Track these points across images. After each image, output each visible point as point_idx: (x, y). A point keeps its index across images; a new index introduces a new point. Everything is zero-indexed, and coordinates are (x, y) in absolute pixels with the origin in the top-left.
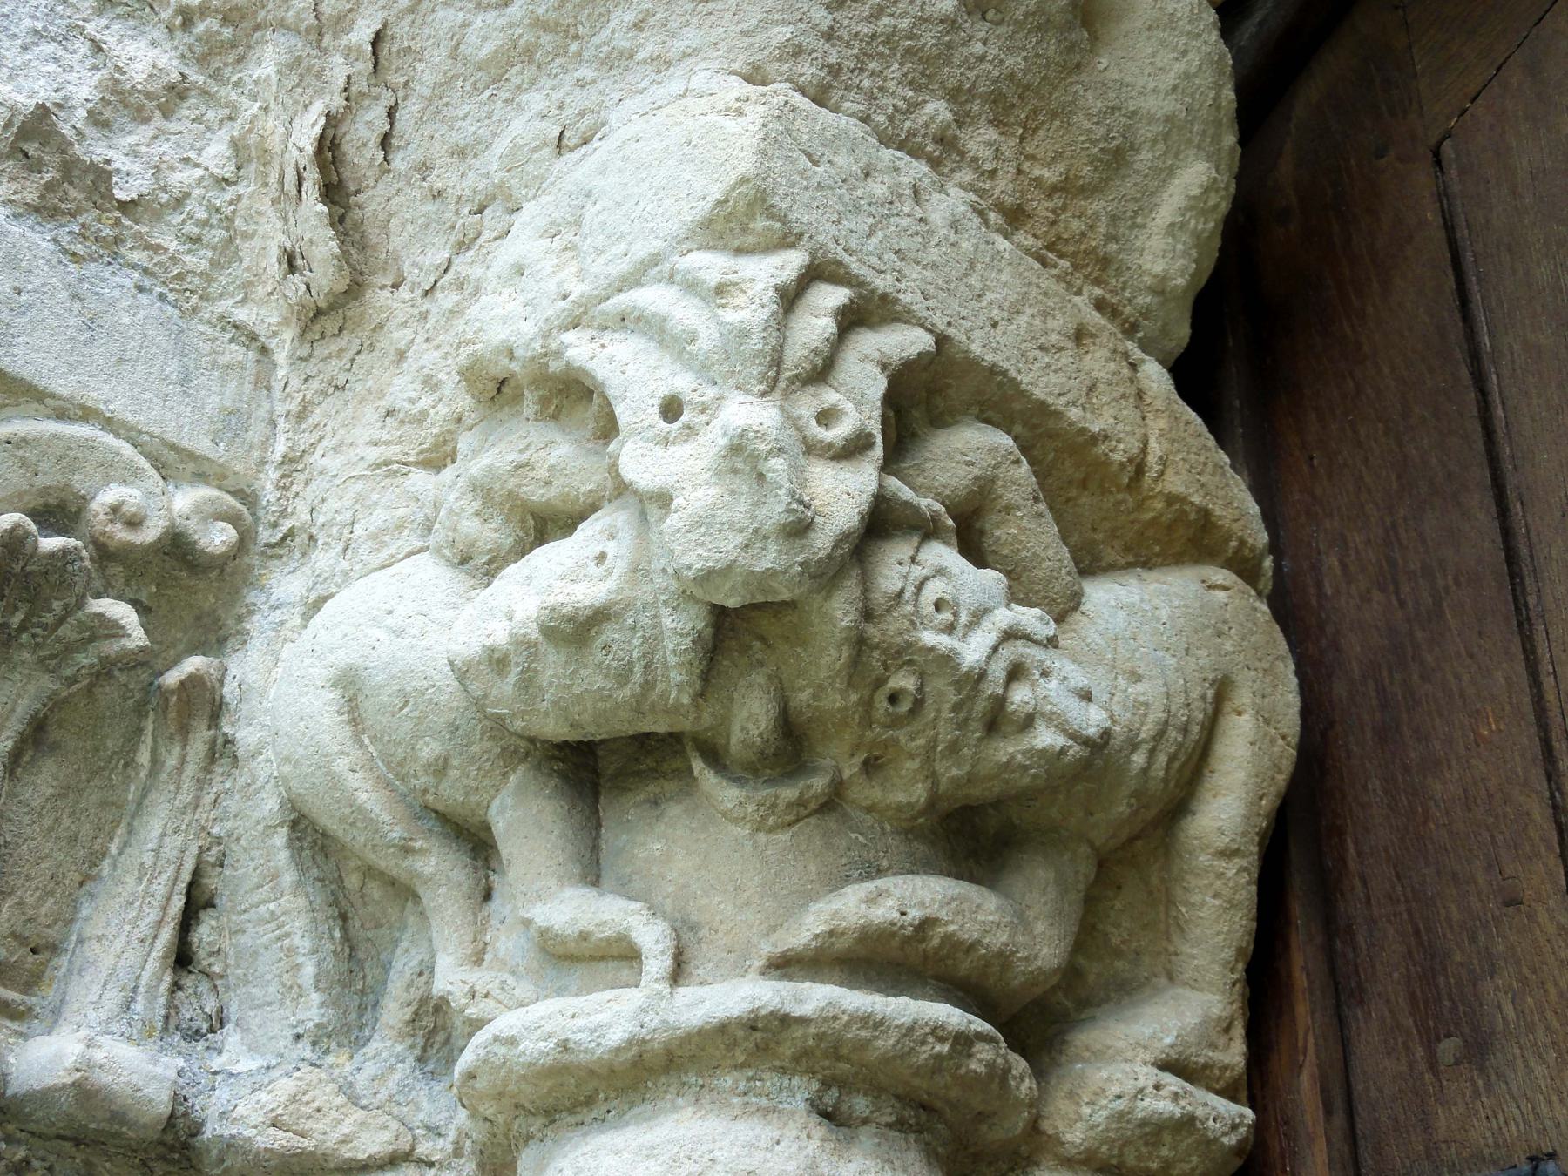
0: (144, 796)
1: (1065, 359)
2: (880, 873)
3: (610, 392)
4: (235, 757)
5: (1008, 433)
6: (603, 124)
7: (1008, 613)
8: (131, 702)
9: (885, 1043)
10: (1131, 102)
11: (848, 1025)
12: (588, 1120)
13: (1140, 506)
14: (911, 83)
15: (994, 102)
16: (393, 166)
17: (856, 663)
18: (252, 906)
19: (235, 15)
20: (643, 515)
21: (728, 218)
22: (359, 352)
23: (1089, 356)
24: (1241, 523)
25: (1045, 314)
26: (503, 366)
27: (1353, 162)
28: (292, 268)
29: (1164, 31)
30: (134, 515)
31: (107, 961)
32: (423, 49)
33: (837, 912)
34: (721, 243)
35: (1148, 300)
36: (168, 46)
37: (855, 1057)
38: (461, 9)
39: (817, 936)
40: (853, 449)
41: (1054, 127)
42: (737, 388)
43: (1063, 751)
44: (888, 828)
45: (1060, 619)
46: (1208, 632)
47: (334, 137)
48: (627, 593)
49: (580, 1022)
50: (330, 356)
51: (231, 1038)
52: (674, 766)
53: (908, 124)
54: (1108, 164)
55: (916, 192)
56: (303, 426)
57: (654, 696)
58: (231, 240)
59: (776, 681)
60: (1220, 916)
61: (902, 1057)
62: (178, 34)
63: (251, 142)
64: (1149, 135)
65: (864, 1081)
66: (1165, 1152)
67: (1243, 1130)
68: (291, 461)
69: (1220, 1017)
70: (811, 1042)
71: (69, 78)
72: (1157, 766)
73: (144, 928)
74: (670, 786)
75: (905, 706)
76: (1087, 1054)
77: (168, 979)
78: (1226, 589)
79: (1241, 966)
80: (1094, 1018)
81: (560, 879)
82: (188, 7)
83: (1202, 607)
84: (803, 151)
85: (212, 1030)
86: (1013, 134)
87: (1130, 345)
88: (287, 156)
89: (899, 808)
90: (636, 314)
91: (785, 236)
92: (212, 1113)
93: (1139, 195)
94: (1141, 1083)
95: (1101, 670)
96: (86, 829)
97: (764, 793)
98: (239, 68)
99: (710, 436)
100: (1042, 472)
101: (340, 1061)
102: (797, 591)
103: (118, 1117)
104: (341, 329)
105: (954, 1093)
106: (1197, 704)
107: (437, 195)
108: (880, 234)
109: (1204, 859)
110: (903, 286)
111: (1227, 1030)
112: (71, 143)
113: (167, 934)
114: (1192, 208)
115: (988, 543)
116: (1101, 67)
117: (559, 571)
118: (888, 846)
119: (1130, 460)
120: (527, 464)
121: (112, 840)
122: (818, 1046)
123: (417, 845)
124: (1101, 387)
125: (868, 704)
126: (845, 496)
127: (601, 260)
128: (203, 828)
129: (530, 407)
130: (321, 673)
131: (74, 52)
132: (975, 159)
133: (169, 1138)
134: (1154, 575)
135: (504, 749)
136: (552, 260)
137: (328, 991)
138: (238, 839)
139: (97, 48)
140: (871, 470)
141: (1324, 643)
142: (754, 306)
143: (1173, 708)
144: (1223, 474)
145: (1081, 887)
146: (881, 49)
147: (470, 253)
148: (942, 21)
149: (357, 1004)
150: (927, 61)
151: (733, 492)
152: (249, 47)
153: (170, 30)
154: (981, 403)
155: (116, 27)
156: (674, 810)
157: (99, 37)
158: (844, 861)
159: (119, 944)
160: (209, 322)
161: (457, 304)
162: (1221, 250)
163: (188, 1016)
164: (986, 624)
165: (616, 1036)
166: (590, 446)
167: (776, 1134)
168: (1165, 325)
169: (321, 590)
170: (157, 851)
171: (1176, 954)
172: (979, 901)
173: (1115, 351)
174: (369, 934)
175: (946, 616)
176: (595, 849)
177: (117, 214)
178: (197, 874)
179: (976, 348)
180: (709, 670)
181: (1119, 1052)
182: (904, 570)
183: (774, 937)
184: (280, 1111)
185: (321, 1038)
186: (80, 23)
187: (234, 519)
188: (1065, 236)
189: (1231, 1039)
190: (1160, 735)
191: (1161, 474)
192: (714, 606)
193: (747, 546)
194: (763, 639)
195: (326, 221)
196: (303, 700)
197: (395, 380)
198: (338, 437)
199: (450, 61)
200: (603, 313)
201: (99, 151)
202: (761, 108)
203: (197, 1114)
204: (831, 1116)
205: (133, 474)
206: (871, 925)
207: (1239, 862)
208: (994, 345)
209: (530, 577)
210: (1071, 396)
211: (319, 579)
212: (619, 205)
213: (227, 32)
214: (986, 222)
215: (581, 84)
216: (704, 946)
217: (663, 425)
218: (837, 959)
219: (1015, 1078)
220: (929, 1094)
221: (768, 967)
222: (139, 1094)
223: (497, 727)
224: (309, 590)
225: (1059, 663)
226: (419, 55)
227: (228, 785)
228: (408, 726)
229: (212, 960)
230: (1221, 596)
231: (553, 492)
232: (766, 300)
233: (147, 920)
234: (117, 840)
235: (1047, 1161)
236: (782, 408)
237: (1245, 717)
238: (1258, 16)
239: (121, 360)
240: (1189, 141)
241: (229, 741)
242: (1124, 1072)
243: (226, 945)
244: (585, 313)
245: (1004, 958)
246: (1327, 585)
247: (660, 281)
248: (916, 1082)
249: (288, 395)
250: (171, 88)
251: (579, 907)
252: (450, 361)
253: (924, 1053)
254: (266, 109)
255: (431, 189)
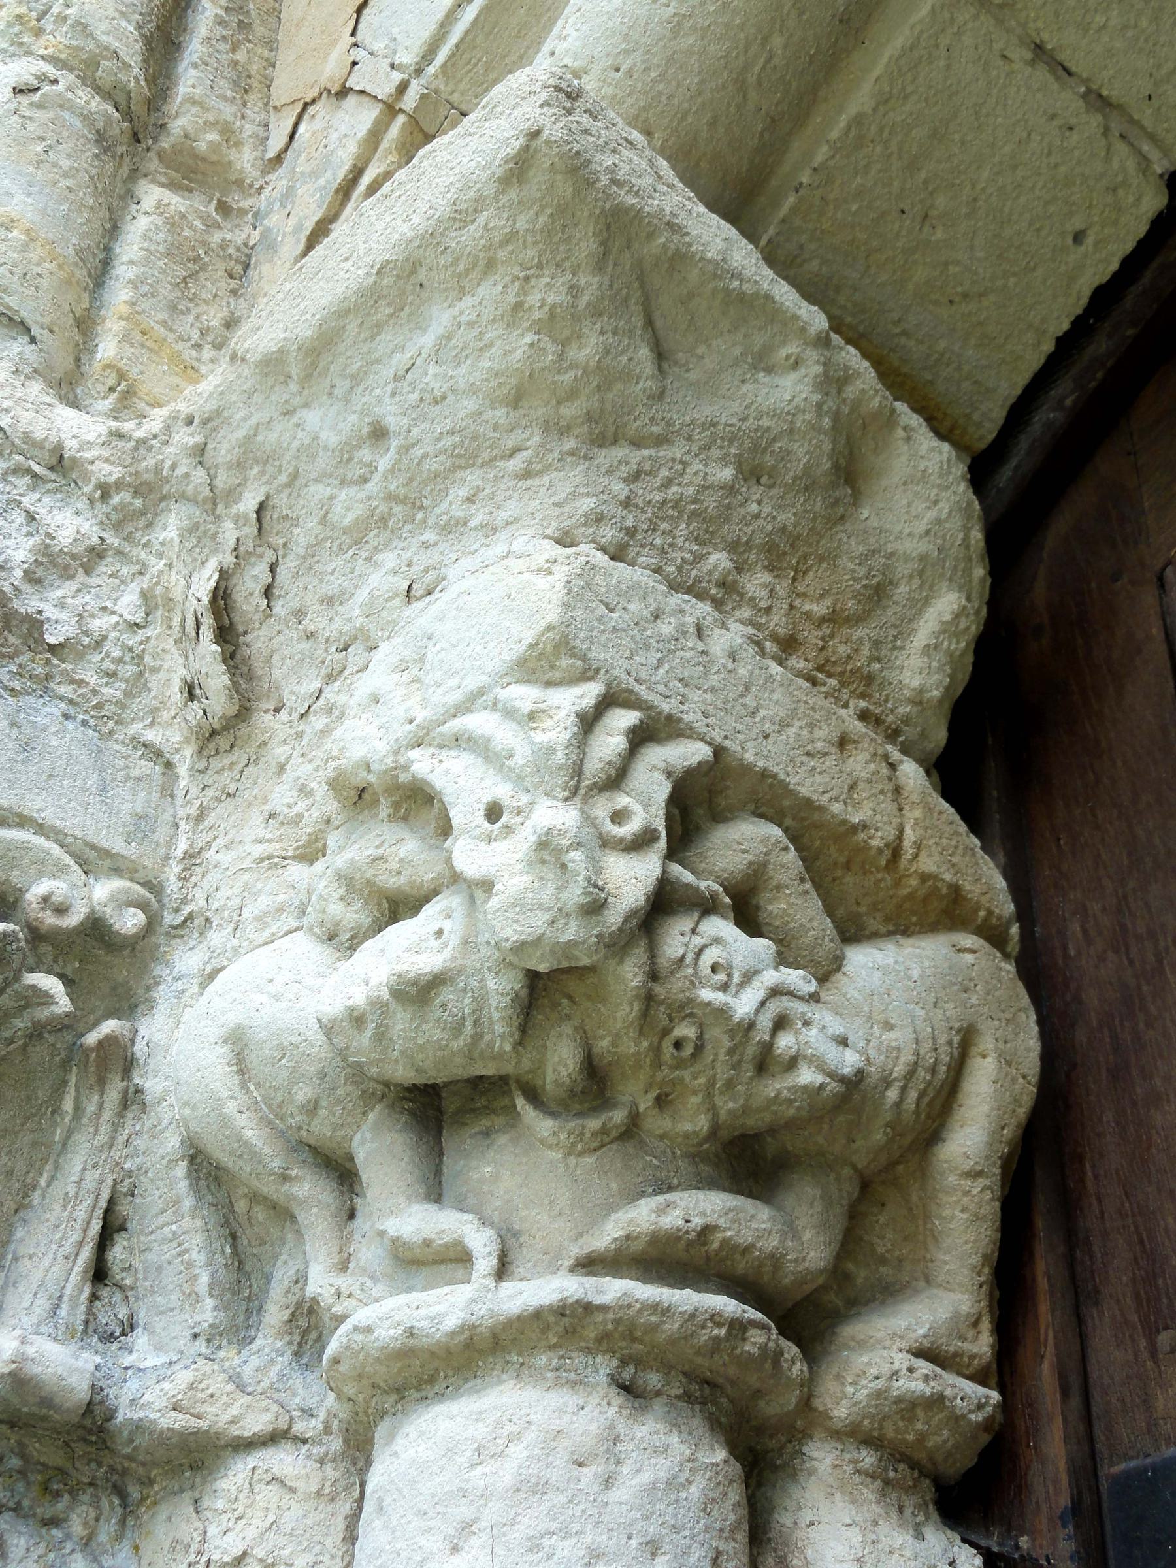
0: (68, 1137)
1: (829, 762)
2: (671, 1189)
3: (446, 799)
4: (144, 1104)
5: (779, 825)
6: (444, 579)
7: (776, 974)
8: (58, 1059)
9: (672, 1327)
10: (889, 545)
11: (640, 1311)
12: (431, 1395)
13: (897, 884)
14: (697, 539)
15: (768, 551)
16: (274, 611)
17: (645, 1014)
18: (157, 1228)
19: (144, 489)
20: (472, 897)
21: (539, 657)
22: (247, 765)
23: (852, 759)
24: (988, 896)
25: (812, 726)
26: (363, 778)
27: (1093, 585)
28: (192, 696)
29: (918, 484)
30: (62, 903)
31: (38, 1274)
32: (298, 517)
33: (632, 1220)
34: (534, 677)
35: (908, 709)
36: (89, 515)
37: (647, 1338)
38: (329, 485)
39: (615, 1240)
40: (641, 842)
41: (821, 569)
42: (546, 795)
43: (822, 1087)
44: (679, 1153)
45: (823, 979)
46: (955, 988)
47: (226, 588)
48: (459, 961)
49: (423, 1312)
50: (223, 769)
51: (140, 1339)
52: (503, 1104)
53: (694, 572)
54: (870, 598)
55: (700, 631)
56: (201, 827)
57: (482, 1045)
58: (141, 674)
59: (581, 1031)
60: (968, 1227)
61: (685, 1338)
62: (98, 505)
63: (158, 593)
64: (906, 572)
65: (655, 1359)
66: (919, 1426)
67: (989, 1409)
68: (191, 857)
69: (969, 1313)
70: (610, 1326)
71: (8, 544)
72: (909, 1100)
73: (68, 1247)
74: (499, 1121)
75: (688, 1051)
76: (853, 1343)
77: (87, 1290)
78: (974, 952)
79: (986, 1270)
80: (859, 1314)
81: (409, 1198)
82: (106, 483)
83: (950, 968)
84: (601, 601)
85: (124, 1334)
86: (786, 577)
87: (889, 748)
88: (187, 604)
89: (687, 1136)
90: (467, 735)
91: (585, 671)
92: (124, 1400)
93: (898, 622)
94: (896, 1366)
95: (859, 1021)
96: (21, 1165)
97: (573, 1124)
98: (147, 532)
99: (524, 834)
100: (808, 858)
101: (230, 1355)
102: (595, 958)
103: (47, 1402)
104: (232, 746)
105: (732, 1371)
106: (943, 1049)
107: (310, 636)
108: (666, 666)
109: (952, 1179)
110: (686, 708)
111: (976, 1324)
112: (10, 599)
113: (87, 1252)
114: (945, 631)
115: (763, 917)
116: (863, 517)
117: (406, 944)
118: (678, 1168)
119: (887, 845)
120: (382, 858)
121: (41, 1174)
122: (616, 1329)
123: (294, 1173)
124: (861, 785)
125: (657, 1050)
126: (633, 881)
127: (440, 691)
128: (117, 1164)
129: (384, 811)
130: (215, 1032)
131: (13, 522)
132: (753, 599)
133: (88, 1422)
134: (910, 941)
135: (363, 1092)
136: (402, 690)
137: (220, 1296)
138: (146, 1172)
139: (31, 518)
140: (656, 859)
141: (1068, 998)
142: (559, 729)
143: (922, 1052)
144: (974, 855)
145: (845, 1202)
146: (670, 512)
147: (337, 684)
148: (721, 488)
149: (244, 1308)
150: (710, 520)
151: (542, 879)
152: (156, 514)
153: (91, 501)
154: (757, 801)
155: (47, 500)
156: (502, 1139)
157: (32, 508)
158: (640, 1179)
159: (47, 1261)
160: (123, 742)
161: (327, 725)
162: (975, 665)
163: (104, 1322)
164: (756, 983)
165: (451, 1323)
166: (432, 842)
167: (581, 1402)
168: (923, 730)
169: (215, 964)
170: (79, 1183)
171: (932, 1261)
172: (753, 1212)
173: (875, 754)
174: (255, 1251)
175: (721, 977)
176: (438, 1173)
177: (48, 655)
178: (111, 1202)
179: (749, 757)
180: (526, 1023)
181: (879, 1341)
182: (686, 939)
183: (581, 1241)
184: (180, 1397)
185: (214, 1337)
186: (18, 498)
187: (143, 906)
188: (833, 659)
189: (979, 1333)
190: (911, 1074)
191: (916, 856)
192: (529, 971)
193: (553, 922)
194: (570, 998)
195: (219, 659)
196: (200, 1054)
197: (277, 789)
198: (229, 836)
199: (320, 527)
200: (441, 735)
201: (32, 603)
202: (566, 568)
203: (112, 1401)
204: (628, 1389)
205: (60, 870)
206: (660, 1229)
207: (982, 1182)
208: (765, 753)
209: (383, 950)
210: (834, 793)
211: (213, 954)
212: (454, 646)
213: (138, 503)
214: (762, 652)
215: (426, 546)
216: (525, 1250)
217: (487, 825)
218: (633, 1259)
219: (786, 1360)
220: (711, 1372)
221: (577, 1266)
222: (64, 1383)
223: (357, 1073)
224: (205, 964)
225: (820, 1015)
226: (295, 522)
227: (138, 1128)
228: (285, 1074)
229: (124, 1274)
230: (969, 958)
231: (402, 880)
232: (568, 724)
233: (70, 1241)
234: (45, 1175)
235: (819, 1434)
236: (582, 811)
237: (989, 1059)
238: (1013, 462)
239: (50, 776)
240: (942, 575)
241: (139, 1091)
242: (882, 1357)
243: (136, 1261)
244: (427, 734)
245: (776, 1260)
246: (1070, 946)
247: (486, 708)
248: (699, 1360)
249: (189, 802)
250: (92, 549)
251: (423, 1219)
252: (321, 773)
253: (704, 1336)
254: (170, 566)
255: (305, 631)
